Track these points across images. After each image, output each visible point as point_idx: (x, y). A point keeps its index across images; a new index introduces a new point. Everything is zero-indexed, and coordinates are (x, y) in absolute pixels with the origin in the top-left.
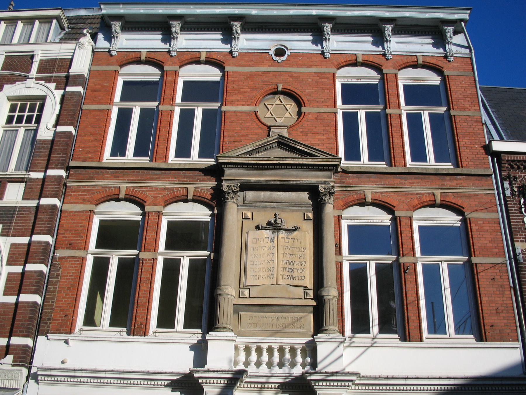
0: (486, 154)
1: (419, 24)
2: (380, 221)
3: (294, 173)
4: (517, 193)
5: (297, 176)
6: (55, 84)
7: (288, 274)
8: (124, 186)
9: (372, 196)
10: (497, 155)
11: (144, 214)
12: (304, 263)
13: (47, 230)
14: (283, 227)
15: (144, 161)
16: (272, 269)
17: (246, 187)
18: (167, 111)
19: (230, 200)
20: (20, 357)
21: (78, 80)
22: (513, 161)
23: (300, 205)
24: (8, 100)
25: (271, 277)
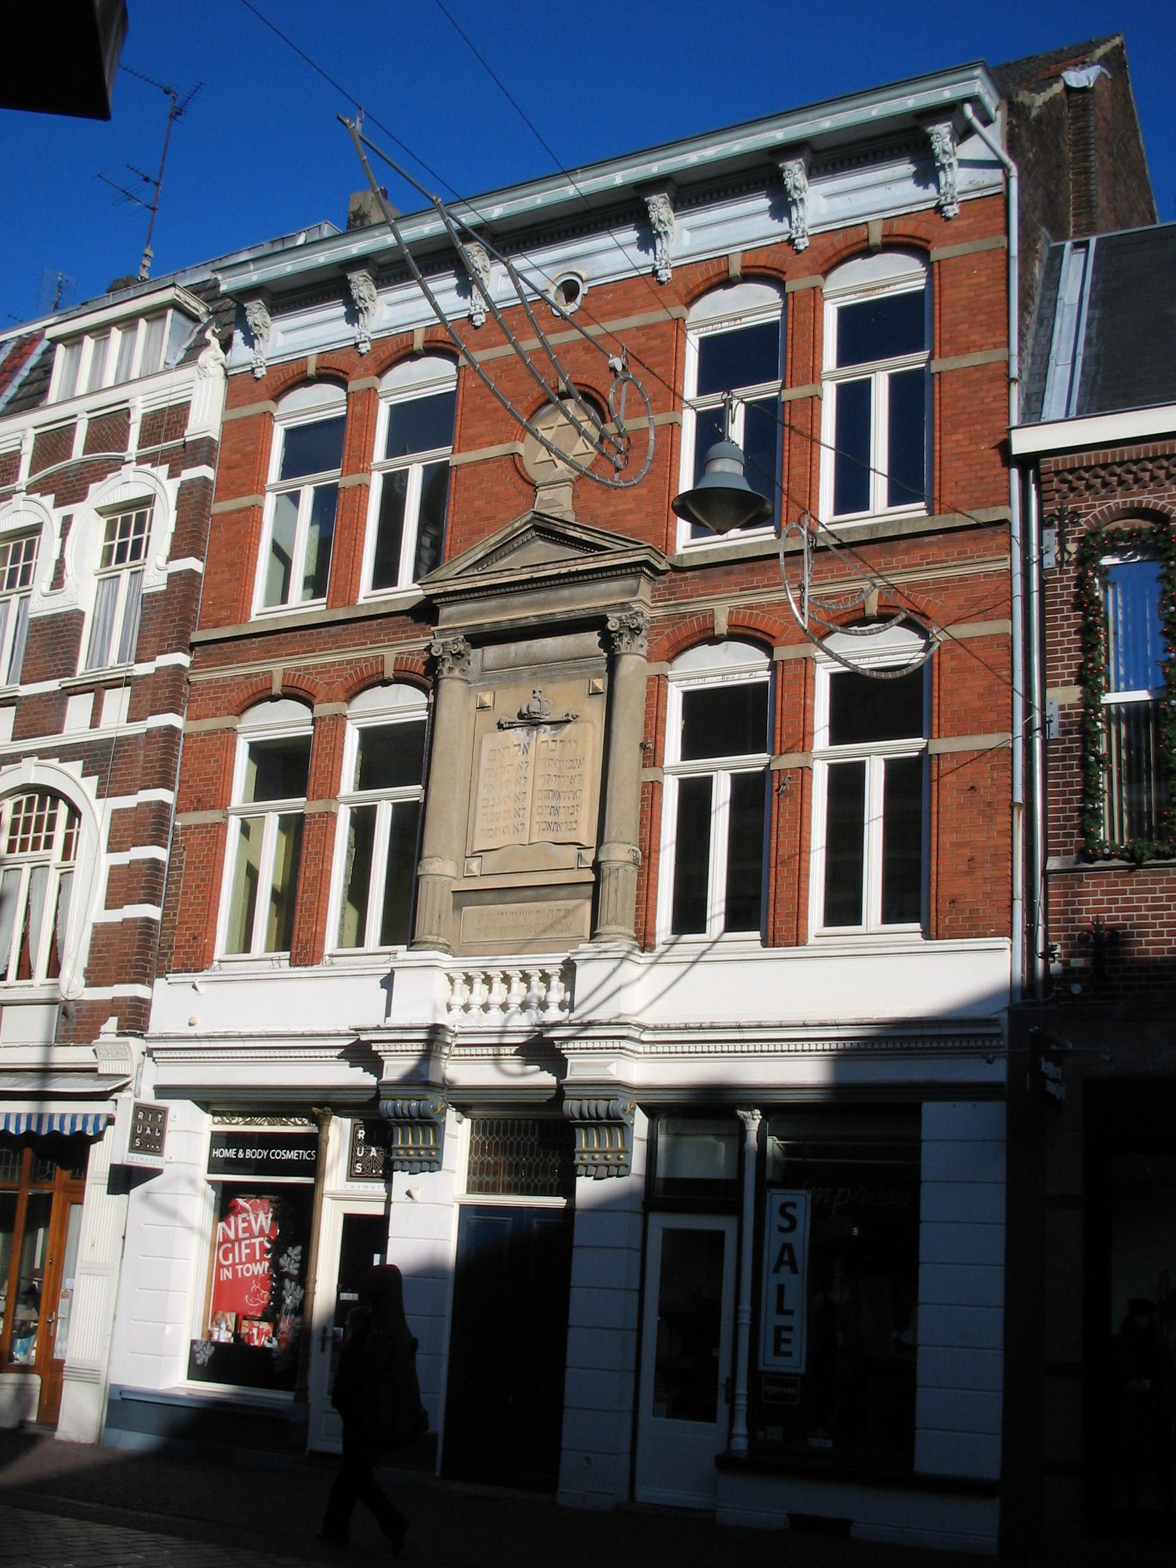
0: (1004, 466)
1: (870, 133)
2: (747, 675)
3: (565, 593)
4: (1074, 556)
5: (570, 601)
6: (53, 495)
7: (550, 819)
8: (278, 669)
9: (730, 619)
10: (1029, 462)
11: (773, 667)
12: (579, 793)
13: (160, 779)
14: (547, 719)
15: (318, 609)
16: (521, 812)
17: (480, 639)
18: (802, 400)
19: (623, 650)
20: (127, 1020)
21: (200, 451)
22: (1072, 471)
23: (582, 663)
24: (101, 514)
25: (520, 828)
